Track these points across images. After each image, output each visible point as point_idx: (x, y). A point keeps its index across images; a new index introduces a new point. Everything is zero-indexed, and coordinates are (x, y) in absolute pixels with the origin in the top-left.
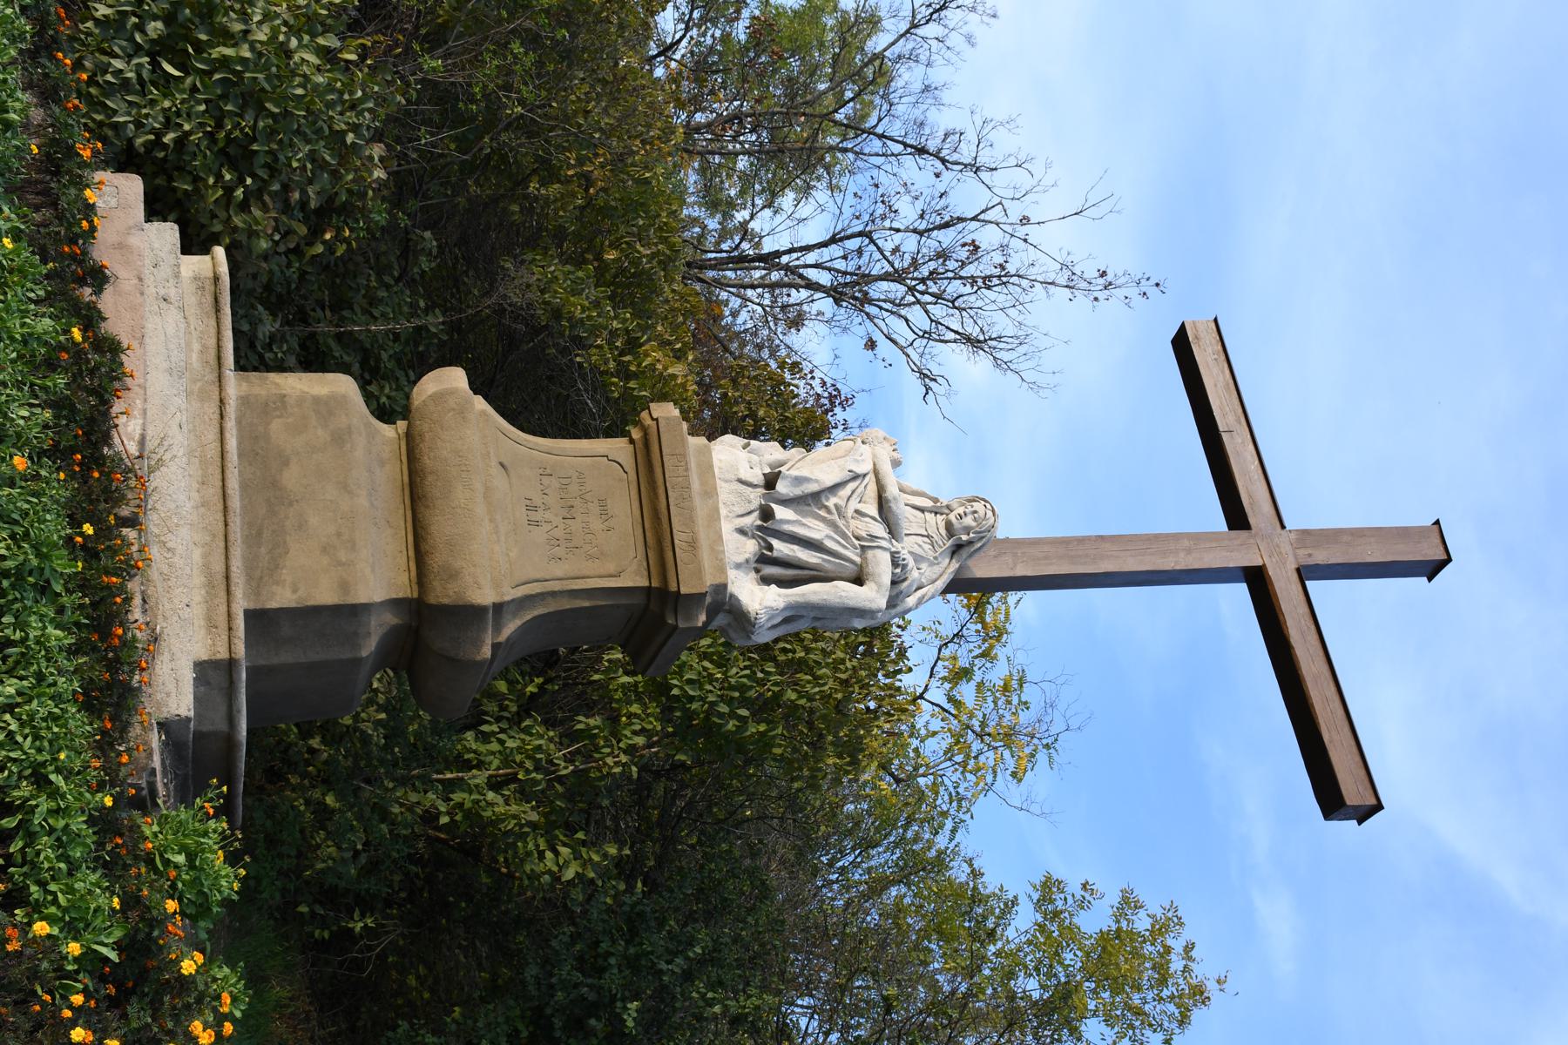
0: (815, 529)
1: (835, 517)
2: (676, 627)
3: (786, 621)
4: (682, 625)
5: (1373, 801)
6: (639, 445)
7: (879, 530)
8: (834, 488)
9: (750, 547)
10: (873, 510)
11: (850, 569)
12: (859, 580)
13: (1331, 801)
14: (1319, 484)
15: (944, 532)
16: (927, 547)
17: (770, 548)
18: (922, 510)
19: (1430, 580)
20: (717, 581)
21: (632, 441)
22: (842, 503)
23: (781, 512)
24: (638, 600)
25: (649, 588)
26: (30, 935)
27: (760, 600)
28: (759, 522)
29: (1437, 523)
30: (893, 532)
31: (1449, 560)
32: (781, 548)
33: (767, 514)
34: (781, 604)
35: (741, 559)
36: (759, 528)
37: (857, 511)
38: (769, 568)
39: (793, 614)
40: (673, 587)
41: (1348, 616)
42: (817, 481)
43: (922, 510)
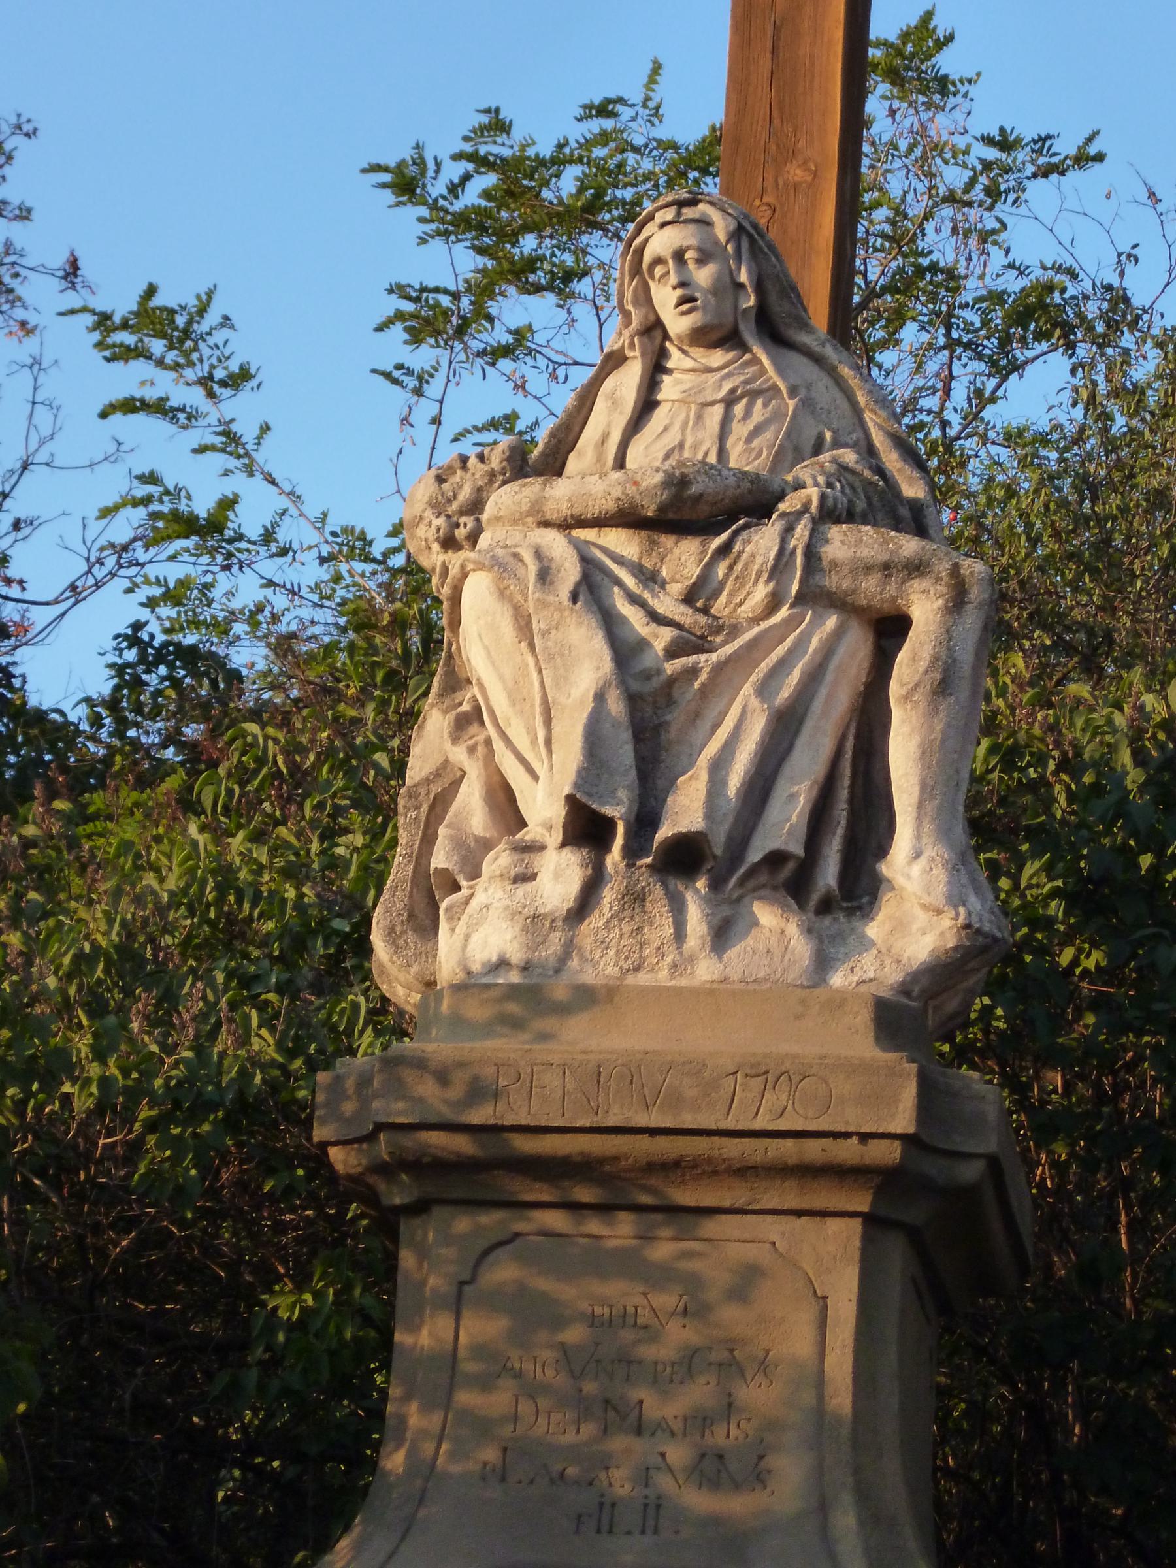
0: (739, 726)
1: (706, 661)
2: (994, 1163)
3: (450, 656)
4: (990, 1144)
7: (762, 542)
8: (625, 652)
9: (775, 927)
10: (684, 558)
11: (857, 647)
15: (718, 357)
16: (759, 412)
17: (776, 859)
18: (647, 405)
20: (863, 1018)
23: (686, 810)
24: (896, 1251)
25: (871, 1221)
26: (288, 975)
27: (920, 908)
30: (756, 503)
32: (786, 821)
33: (684, 857)
36: (716, 885)
37: (689, 599)
40: (888, 1153)
43: (647, 405)
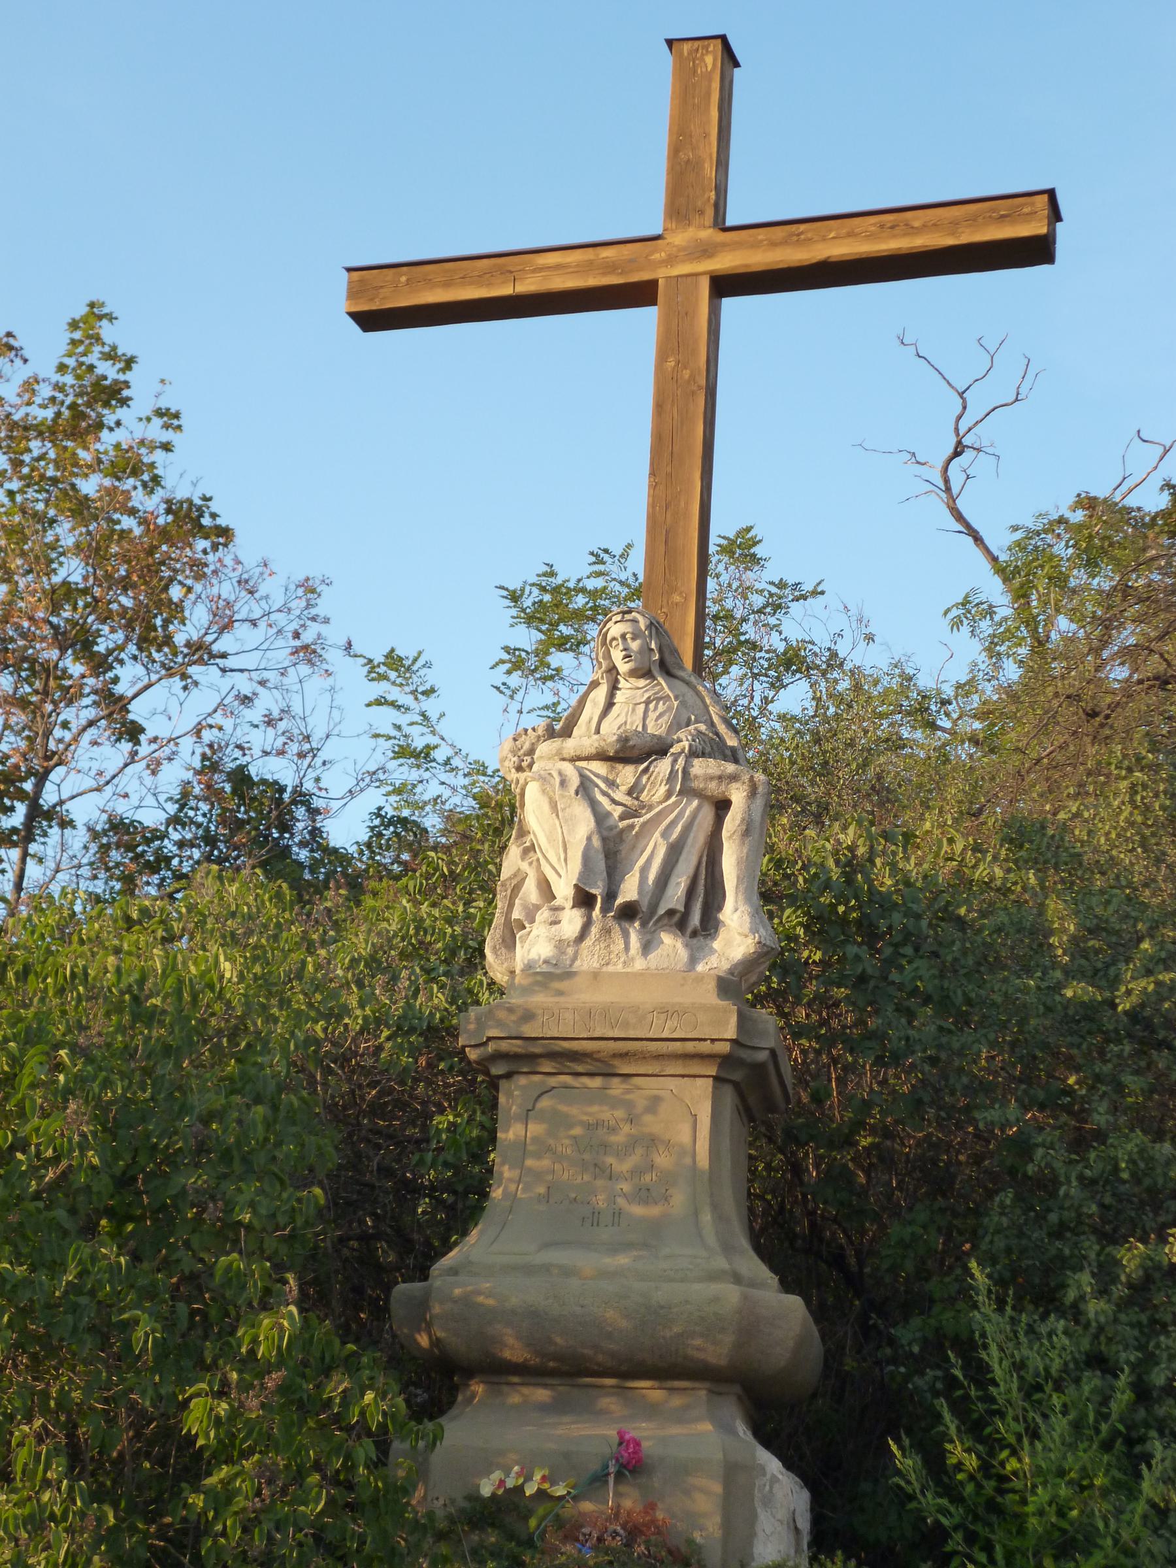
1: (638, 821)
5: (1045, 197)
6: (513, 1067)
10: (627, 774)
12: (722, 806)
13: (1038, 251)
14: (605, 188)
15: (642, 682)
17: (671, 913)
18: (610, 704)
19: (737, 64)
21: (508, 1076)
22: (620, 809)
23: (629, 891)
27: (738, 935)
28: (637, 924)
29: (670, 43)
31: (723, 39)
32: (676, 895)
33: (629, 912)
34: (744, 909)
35: (683, 953)
37: (629, 793)
38: (698, 919)
39: (769, 897)
40: (725, 1048)
41: (765, 187)
42: (589, 839)
43: (610, 704)
